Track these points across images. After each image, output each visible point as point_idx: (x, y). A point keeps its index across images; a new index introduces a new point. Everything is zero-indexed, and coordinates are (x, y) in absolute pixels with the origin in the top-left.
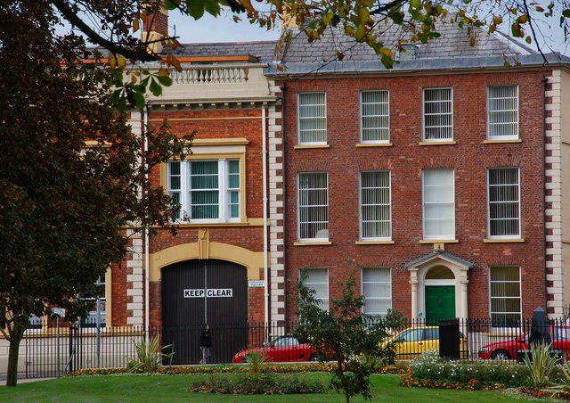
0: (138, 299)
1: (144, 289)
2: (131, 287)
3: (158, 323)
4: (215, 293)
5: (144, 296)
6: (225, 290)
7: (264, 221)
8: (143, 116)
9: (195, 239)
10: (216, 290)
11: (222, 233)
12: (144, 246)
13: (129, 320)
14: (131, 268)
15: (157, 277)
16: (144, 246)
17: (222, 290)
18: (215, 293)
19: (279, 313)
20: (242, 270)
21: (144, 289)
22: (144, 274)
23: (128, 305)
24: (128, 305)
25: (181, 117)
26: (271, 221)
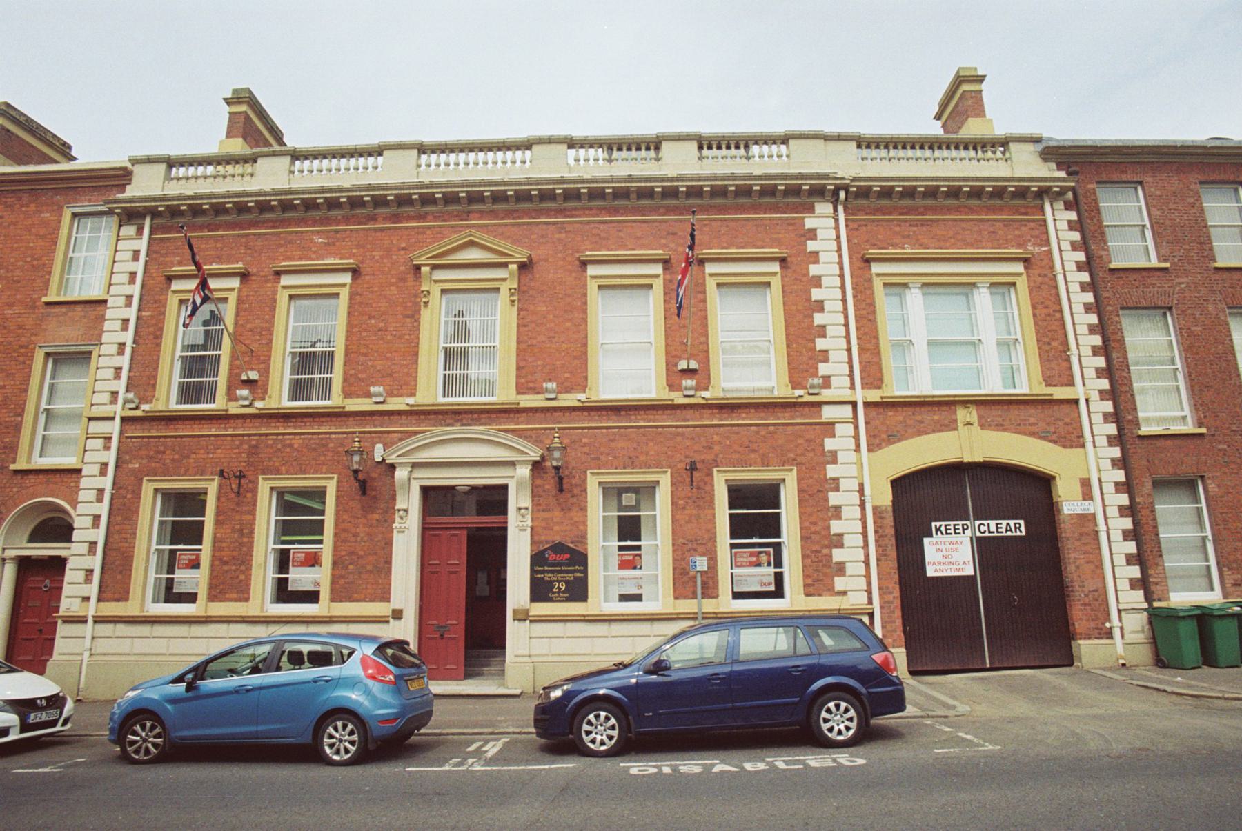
0: (853, 540)
1: (863, 519)
2: (834, 461)
3: (1055, 144)
4: (993, 528)
5: (865, 534)
6: (1012, 522)
7: (1078, 392)
8: (835, 210)
9: (951, 426)
10: (993, 523)
11: (996, 409)
12: (856, 437)
13: (839, 583)
14: (836, 480)
15: (886, 498)
16: (856, 437)
17: (1004, 522)
18: (993, 528)
19: (1129, 563)
20: (1044, 482)
21: (863, 519)
22: (861, 491)
23: (829, 467)
24: (829, 467)
25: (901, 214)
26: (1088, 385)
